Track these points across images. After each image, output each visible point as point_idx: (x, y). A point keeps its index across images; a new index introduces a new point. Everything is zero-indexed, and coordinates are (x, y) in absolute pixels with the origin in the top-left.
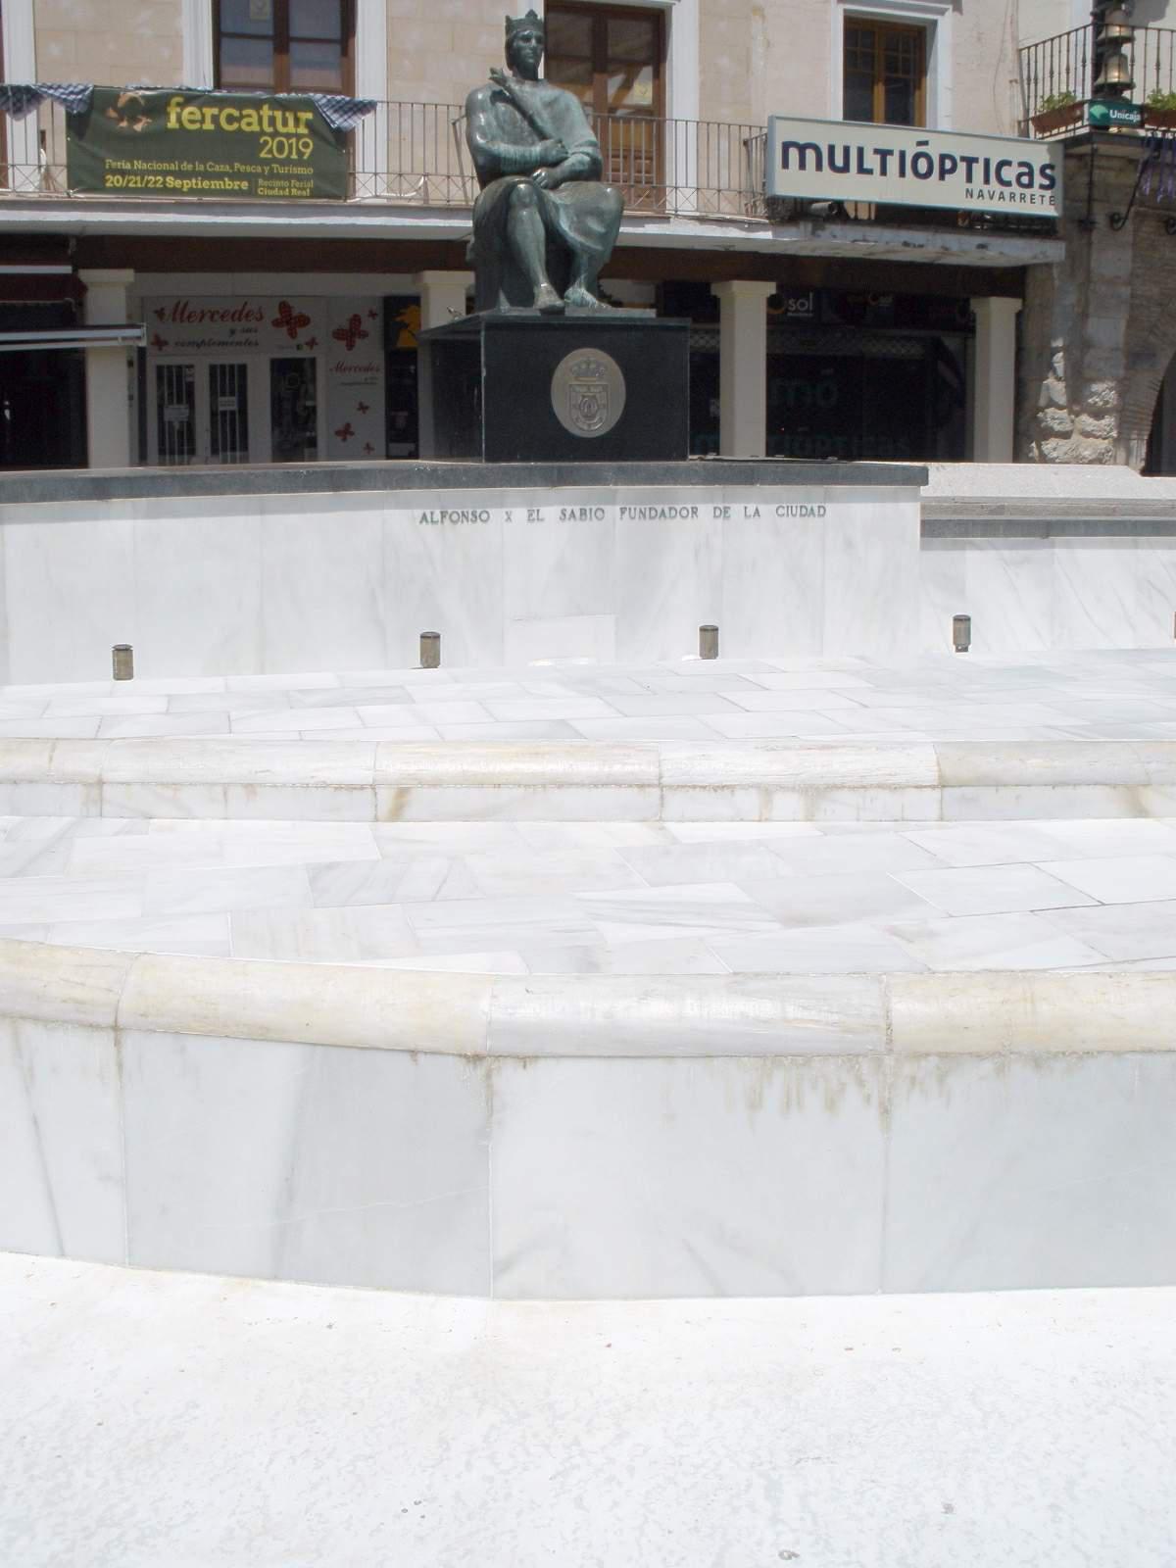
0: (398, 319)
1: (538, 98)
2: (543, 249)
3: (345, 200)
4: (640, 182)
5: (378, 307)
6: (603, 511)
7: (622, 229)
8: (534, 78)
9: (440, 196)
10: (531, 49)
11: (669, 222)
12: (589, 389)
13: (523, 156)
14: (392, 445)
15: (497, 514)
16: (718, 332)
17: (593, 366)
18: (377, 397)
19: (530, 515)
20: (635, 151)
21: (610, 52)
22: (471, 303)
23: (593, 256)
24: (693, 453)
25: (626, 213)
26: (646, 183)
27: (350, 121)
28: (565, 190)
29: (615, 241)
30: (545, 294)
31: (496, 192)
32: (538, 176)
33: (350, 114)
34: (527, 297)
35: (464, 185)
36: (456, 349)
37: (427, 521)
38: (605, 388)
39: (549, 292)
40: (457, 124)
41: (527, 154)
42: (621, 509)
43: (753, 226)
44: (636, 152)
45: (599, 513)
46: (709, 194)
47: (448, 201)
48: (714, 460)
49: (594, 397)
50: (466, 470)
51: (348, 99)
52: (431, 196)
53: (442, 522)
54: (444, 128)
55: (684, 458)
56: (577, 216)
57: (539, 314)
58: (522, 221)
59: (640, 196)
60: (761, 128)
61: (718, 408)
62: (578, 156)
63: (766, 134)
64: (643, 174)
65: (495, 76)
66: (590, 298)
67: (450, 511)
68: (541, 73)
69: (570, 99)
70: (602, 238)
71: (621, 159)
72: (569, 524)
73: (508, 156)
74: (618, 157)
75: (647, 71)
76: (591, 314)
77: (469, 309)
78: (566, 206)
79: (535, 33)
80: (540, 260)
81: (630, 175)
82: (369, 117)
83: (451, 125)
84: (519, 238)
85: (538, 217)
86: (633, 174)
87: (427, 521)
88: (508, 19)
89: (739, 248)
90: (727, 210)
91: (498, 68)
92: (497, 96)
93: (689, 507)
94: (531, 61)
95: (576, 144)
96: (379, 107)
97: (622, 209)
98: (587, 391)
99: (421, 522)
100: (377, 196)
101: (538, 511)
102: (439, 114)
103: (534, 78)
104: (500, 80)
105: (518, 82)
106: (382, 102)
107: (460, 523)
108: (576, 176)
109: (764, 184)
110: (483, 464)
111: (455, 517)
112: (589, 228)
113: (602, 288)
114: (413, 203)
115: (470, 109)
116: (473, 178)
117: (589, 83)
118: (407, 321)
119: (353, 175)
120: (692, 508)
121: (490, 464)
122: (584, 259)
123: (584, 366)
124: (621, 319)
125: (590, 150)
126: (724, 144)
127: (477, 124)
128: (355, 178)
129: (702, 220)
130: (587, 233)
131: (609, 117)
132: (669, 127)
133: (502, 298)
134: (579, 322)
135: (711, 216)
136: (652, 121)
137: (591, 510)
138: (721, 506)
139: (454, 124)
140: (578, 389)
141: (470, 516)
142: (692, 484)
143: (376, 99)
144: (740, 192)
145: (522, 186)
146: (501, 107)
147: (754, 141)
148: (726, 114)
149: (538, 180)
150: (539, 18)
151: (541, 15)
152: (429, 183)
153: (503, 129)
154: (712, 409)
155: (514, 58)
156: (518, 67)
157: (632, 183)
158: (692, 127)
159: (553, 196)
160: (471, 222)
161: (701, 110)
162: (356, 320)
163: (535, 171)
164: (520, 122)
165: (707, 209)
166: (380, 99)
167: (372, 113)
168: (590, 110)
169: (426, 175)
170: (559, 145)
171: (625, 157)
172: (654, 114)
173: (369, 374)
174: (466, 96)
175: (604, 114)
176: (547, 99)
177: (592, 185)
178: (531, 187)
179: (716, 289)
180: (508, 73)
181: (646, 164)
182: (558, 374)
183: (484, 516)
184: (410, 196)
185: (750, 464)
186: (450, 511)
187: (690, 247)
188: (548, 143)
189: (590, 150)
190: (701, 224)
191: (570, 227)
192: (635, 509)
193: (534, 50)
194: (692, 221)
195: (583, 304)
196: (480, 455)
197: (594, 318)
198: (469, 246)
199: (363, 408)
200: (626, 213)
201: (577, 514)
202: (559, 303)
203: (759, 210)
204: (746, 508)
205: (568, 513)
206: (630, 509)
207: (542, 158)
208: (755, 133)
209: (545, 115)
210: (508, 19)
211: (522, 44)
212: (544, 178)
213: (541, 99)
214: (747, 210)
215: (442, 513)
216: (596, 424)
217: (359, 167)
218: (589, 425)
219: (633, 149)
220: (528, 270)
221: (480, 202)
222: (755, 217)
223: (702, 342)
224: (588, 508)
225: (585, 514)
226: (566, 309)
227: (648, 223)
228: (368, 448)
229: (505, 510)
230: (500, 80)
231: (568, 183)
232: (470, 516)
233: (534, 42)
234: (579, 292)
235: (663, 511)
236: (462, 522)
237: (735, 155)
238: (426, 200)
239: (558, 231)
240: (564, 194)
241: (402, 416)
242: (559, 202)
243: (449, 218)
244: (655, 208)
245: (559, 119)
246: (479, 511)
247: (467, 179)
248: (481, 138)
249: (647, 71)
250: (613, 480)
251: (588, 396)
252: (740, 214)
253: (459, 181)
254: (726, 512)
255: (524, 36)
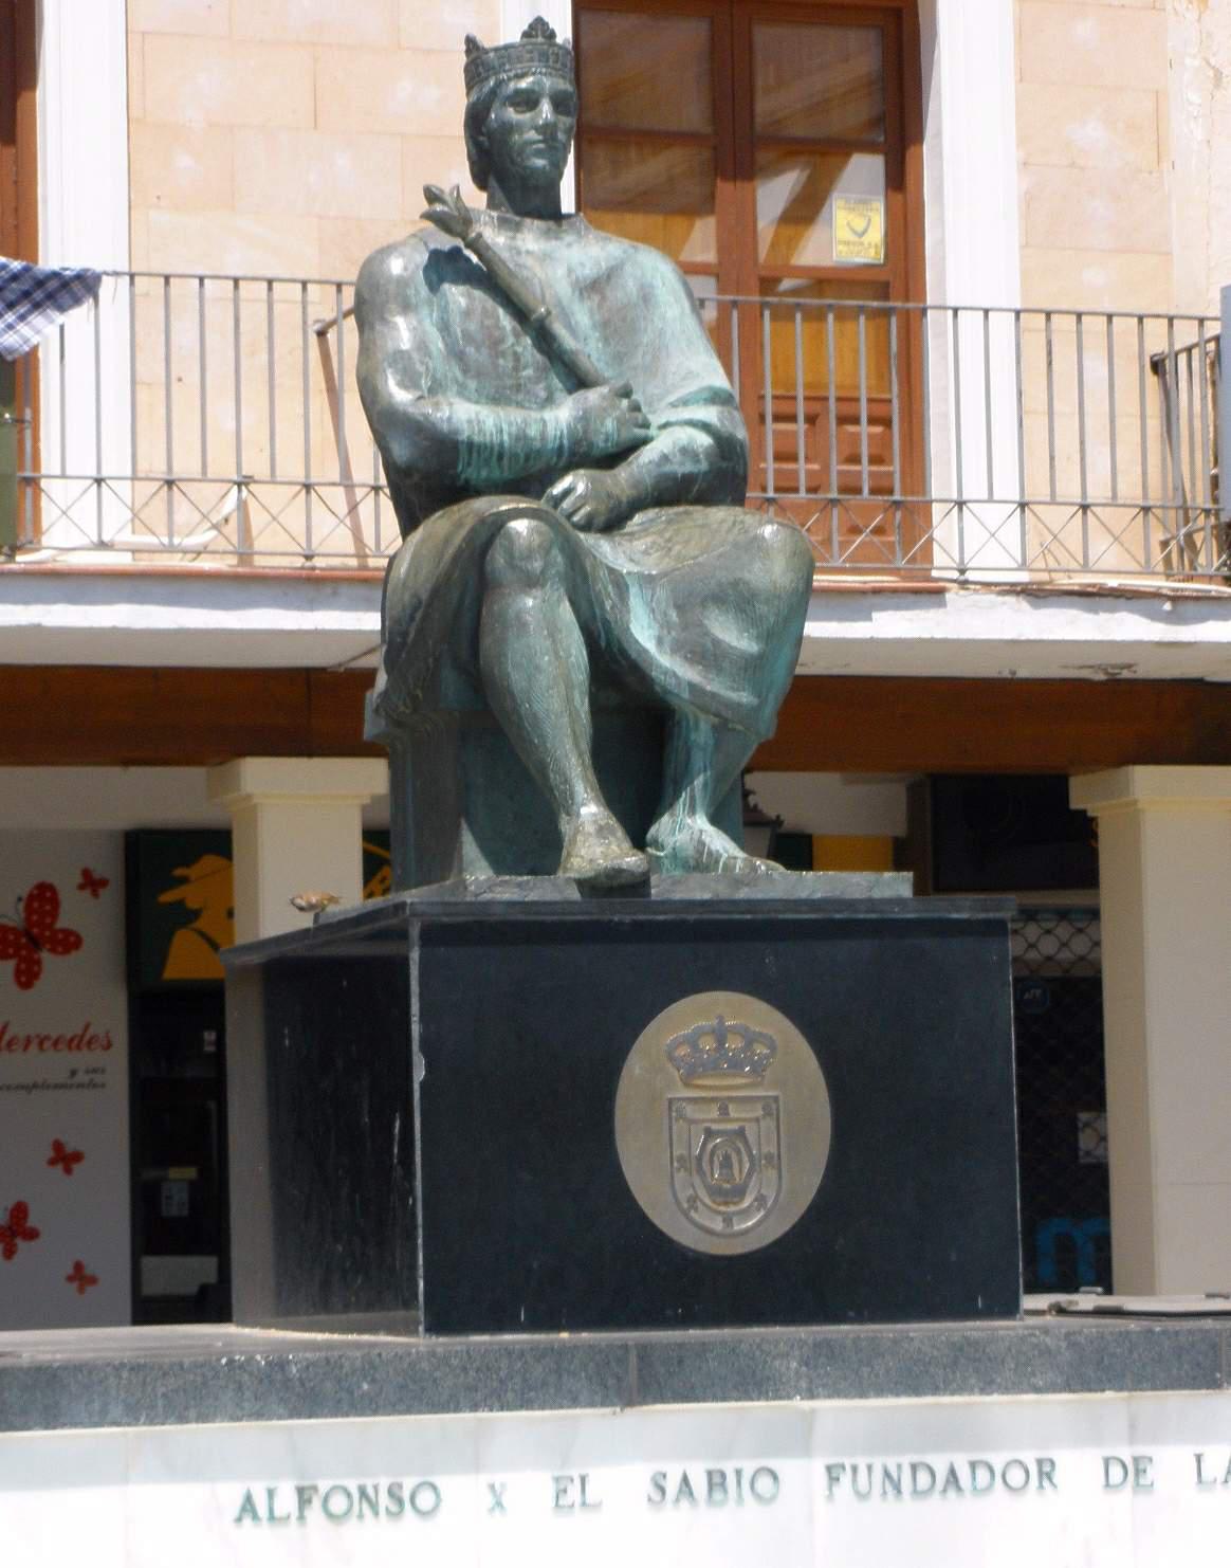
0: (167, 897)
1: (561, 272)
2: (582, 705)
3: (11, 557)
4: (858, 491)
5: (109, 866)
6: (775, 1477)
7: (813, 629)
8: (550, 212)
9: (281, 542)
10: (537, 129)
11: (942, 604)
12: (724, 1111)
13: (521, 437)
14: (149, 1262)
15: (461, 1491)
16: (1094, 914)
17: (734, 1044)
18: (104, 1125)
19: (561, 1492)
20: (839, 399)
21: (764, 106)
22: (380, 851)
23: (725, 722)
24: (1032, 1289)
25: (821, 580)
26: (873, 491)
27: (22, 328)
28: (645, 530)
29: (794, 662)
30: (593, 838)
31: (447, 541)
32: (567, 493)
33: (22, 309)
34: (534, 840)
35: (353, 508)
36: (335, 989)
37: (255, 1517)
38: (770, 1107)
39: (601, 831)
40: (331, 336)
41: (533, 432)
42: (829, 1469)
43: (1183, 606)
44: (841, 410)
45: (764, 1483)
46: (1056, 516)
47: (308, 557)
48: (1100, 1312)
49: (741, 1133)
50: (370, 1366)
51: (16, 265)
52: (258, 545)
53: (301, 1517)
54: (291, 340)
55: (1010, 1309)
56: (679, 608)
57: (574, 894)
58: (523, 625)
59: (855, 530)
60: (1201, 321)
61: (1103, 1139)
62: (677, 437)
63: (1217, 339)
64: (865, 468)
65: (439, 207)
66: (720, 843)
67: (324, 1486)
68: (568, 204)
69: (652, 272)
70: (751, 669)
71: (801, 426)
72: (677, 1516)
73: (476, 439)
74: (792, 418)
75: (866, 168)
76: (724, 892)
77: (373, 866)
78: (647, 581)
79: (547, 82)
80: (577, 745)
81: (826, 468)
82: (77, 318)
83: (313, 339)
84: (517, 680)
85: (566, 612)
86: (836, 467)
87: (255, 1517)
88: (471, 45)
89: (1149, 669)
90: (1114, 558)
91: (445, 185)
92: (445, 267)
93: (1030, 1458)
94: (540, 162)
95: (672, 398)
96: (106, 287)
97: (811, 570)
98: (720, 1116)
99: (239, 1520)
100: (102, 545)
101: (583, 1480)
102: (277, 308)
103: (550, 212)
104: (450, 219)
105: (503, 223)
106: (116, 274)
107: (354, 1519)
108: (673, 492)
109: (1215, 482)
110: (421, 1342)
111: (338, 1504)
112: (716, 642)
113: (752, 800)
114: (206, 564)
115: (369, 305)
116: (376, 489)
117: (706, 205)
118: (192, 904)
119: (33, 482)
120: (1040, 1462)
121: (442, 1339)
122: (701, 734)
123: (708, 1044)
124: (812, 904)
125: (710, 414)
126: (1096, 369)
127: (390, 346)
128: (38, 491)
129: (1036, 594)
130: (708, 655)
131: (763, 305)
132: (936, 327)
133: (469, 847)
134: (692, 917)
135: (1063, 581)
136: (886, 313)
137: (738, 1473)
138: (1126, 1454)
139: (321, 334)
140: (690, 1111)
141: (384, 1500)
142: (1037, 1390)
143: (96, 265)
144: (1146, 510)
145: (520, 526)
146: (458, 295)
147: (1183, 358)
148: (1097, 283)
149: (566, 504)
150: (559, 40)
151: (564, 32)
152: (252, 505)
153: (458, 355)
154: (1085, 1141)
155: (492, 157)
156: (502, 181)
157: (834, 495)
158: (1002, 325)
159: (608, 551)
160: (378, 616)
161: (1026, 274)
162: (43, 898)
163: (552, 482)
164: (511, 340)
165: (1052, 564)
166: (109, 269)
167: (89, 303)
168: (706, 287)
169: (242, 483)
170: (625, 403)
171: (811, 420)
172: (894, 289)
173: (83, 1059)
174: (366, 254)
175: (751, 301)
176: (588, 272)
177: (719, 514)
178: (544, 527)
179: (1083, 794)
180: (475, 198)
181: (871, 437)
182: (636, 1067)
183: (425, 1499)
184: (198, 539)
185: (1209, 1323)
186: (324, 1486)
187: (1006, 674)
188: (593, 396)
189: (710, 414)
190: (1036, 606)
191: (660, 641)
192: (870, 1468)
193: (547, 131)
194: (1011, 599)
195: (700, 862)
196: (409, 1302)
197: (734, 904)
198: (373, 696)
199: (65, 1158)
200: (821, 580)
201: (699, 1484)
202: (632, 860)
203: (1202, 559)
204: (1199, 1458)
205: (672, 1485)
206: (855, 1469)
207: (576, 442)
208: (1186, 334)
209: (582, 316)
210: (471, 45)
211: (511, 114)
212: (584, 499)
213: (570, 271)
214: (1167, 561)
215: (300, 1491)
216: (746, 1214)
217: (49, 462)
218: (728, 1220)
219: (832, 394)
220: (543, 768)
221: (402, 568)
222: (1190, 579)
223: (1048, 946)
224: (729, 1468)
225: (723, 1485)
226: (654, 879)
227: (884, 608)
228: (81, 1277)
229: (484, 1479)
230: (450, 219)
231: (651, 513)
232: (384, 1500)
233: (546, 110)
234: (690, 828)
235: (952, 1472)
236: (361, 1516)
237: (1128, 404)
238: (245, 556)
239: (623, 652)
240: (640, 545)
241: (180, 1178)
242: (625, 567)
243: (311, 605)
244: (902, 564)
245: (621, 327)
246: (409, 1484)
247: (359, 493)
248: (402, 385)
249: (866, 168)
250: (804, 1384)
251: (719, 1133)
252: (1148, 571)
253: (337, 497)
254: (1139, 1472)
255: (518, 92)
